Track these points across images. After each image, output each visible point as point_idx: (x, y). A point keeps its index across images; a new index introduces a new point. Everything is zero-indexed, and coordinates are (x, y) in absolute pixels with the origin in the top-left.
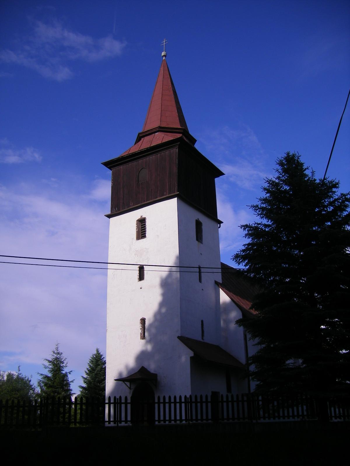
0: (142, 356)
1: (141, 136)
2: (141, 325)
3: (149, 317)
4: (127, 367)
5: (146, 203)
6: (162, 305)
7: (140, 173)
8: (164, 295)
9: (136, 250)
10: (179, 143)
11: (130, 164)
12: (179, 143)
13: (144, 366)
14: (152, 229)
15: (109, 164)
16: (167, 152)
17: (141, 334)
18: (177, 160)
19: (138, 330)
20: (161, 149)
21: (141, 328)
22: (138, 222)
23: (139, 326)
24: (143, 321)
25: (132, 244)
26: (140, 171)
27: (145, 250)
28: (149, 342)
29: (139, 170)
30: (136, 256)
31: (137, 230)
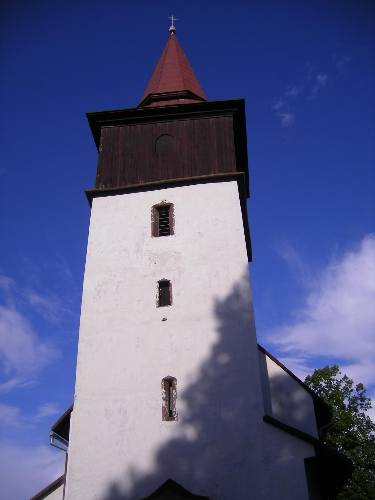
0: (169, 453)
1: (152, 98)
2: (165, 391)
3: (185, 373)
4: (132, 472)
5: (171, 180)
6: (217, 349)
7: (164, 136)
8: (222, 330)
9: (151, 253)
10: (237, 109)
11: (139, 126)
12: (237, 109)
13: (174, 479)
14: (188, 223)
15: (97, 121)
16: (212, 120)
17: (165, 409)
18: (232, 131)
19: (158, 400)
20: (204, 112)
21: (164, 396)
22: (155, 209)
23: (159, 393)
24: (169, 383)
25: (143, 242)
26: (159, 137)
27: (174, 254)
28: (187, 421)
29: (158, 136)
30: (153, 262)
31: (153, 221)
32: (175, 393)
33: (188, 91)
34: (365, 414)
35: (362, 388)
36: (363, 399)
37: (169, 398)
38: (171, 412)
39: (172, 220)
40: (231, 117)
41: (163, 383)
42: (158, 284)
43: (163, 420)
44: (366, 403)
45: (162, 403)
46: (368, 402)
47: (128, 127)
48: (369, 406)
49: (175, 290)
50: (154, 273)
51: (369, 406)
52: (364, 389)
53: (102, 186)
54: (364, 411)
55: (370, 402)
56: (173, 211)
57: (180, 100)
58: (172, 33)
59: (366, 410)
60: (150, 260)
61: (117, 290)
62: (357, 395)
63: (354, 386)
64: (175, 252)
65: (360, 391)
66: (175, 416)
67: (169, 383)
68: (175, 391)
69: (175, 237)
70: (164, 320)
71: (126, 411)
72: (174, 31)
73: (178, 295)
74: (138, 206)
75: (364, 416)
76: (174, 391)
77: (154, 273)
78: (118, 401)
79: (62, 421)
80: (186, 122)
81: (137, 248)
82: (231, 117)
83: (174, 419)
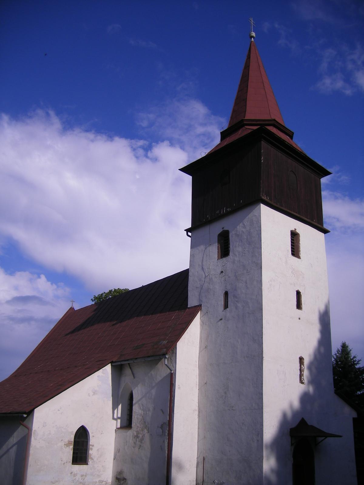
24: (301, 359)
66: (304, 382)
68: (304, 366)
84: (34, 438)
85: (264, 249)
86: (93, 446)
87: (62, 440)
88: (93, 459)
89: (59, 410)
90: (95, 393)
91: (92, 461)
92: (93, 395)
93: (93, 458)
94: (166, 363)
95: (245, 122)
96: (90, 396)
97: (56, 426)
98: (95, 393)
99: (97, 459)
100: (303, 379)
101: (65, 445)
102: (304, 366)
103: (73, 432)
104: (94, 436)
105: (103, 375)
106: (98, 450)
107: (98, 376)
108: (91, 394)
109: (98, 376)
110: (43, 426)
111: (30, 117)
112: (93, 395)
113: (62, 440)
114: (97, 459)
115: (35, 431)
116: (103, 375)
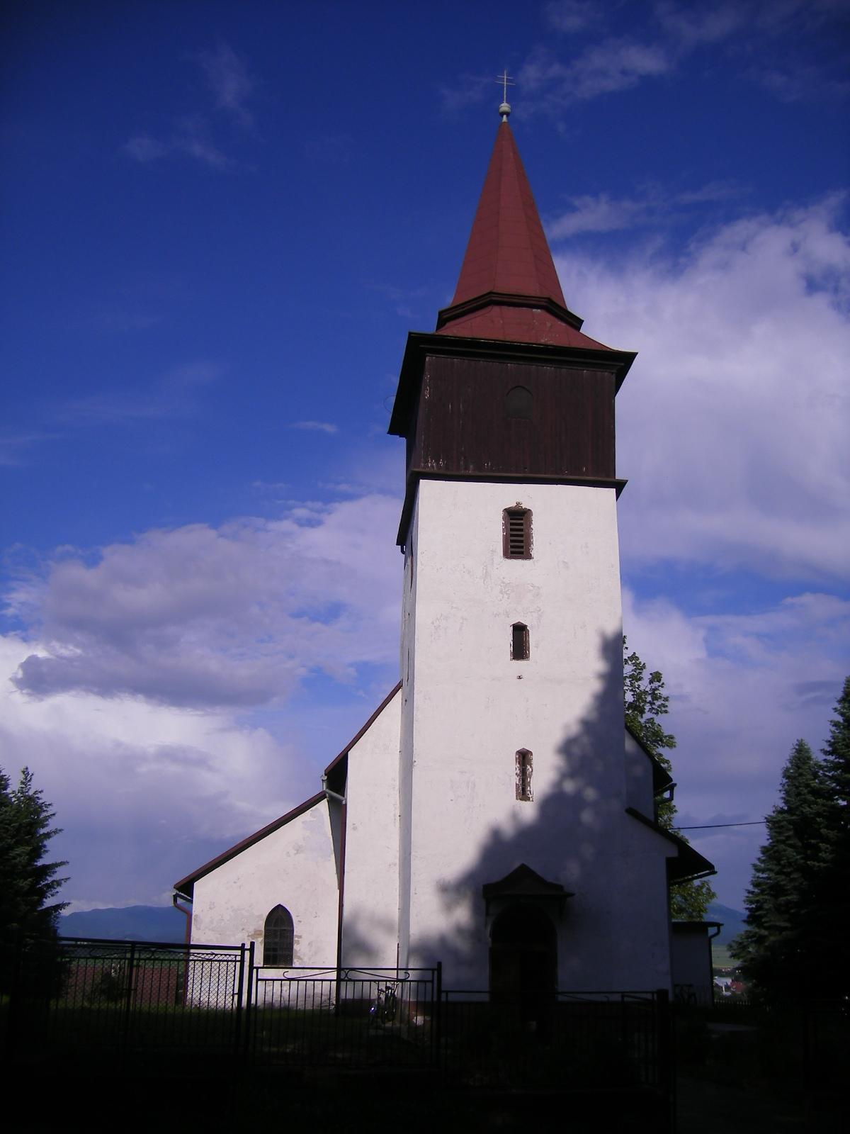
11: (482, 363)
22: (506, 514)
23: (513, 767)
24: (524, 758)
25: (493, 563)
30: (506, 596)
32: (530, 770)
33: (549, 299)
34: (655, 721)
35: (659, 681)
36: (655, 697)
37: (524, 776)
38: (524, 790)
39: (529, 536)
40: (612, 373)
41: (517, 756)
42: (512, 627)
43: (517, 799)
44: (660, 703)
45: (515, 780)
46: (663, 702)
47: (466, 361)
48: (663, 709)
49: (533, 639)
50: (507, 612)
51: (663, 709)
52: (661, 682)
53: (432, 461)
54: (654, 716)
55: (667, 703)
56: (530, 522)
57: (534, 310)
58: (505, 116)
59: (657, 713)
60: (501, 592)
61: (460, 629)
62: (648, 689)
63: (646, 675)
64: (533, 586)
65: (656, 684)
66: (530, 796)
67: (524, 758)
68: (531, 767)
69: (534, 563)
70: (520, 678)
71: (475, 786)
72: (507, 114)
73: (537, 647)
74: (485, 502)
75: (653, 724)
76: (529, 767)
77: (507, 612)
78: (465, 772)
79: (337, 761)
80: (548, 369)
81: (485, 571)
82: (612, 373)
83: (529, 799)
84: (197, 927)
85: (422, 565)
86: (300, 937)
87: (243, 929)
88: (301, 959)
89: (235, 882)
90: (298, 850)
91: (300, 961)
92: (295, 854)
93: (302, 957)
94: (784, 838)
95: (445, 317)
96: (289, 856)
97: (232, 907)
98: (298, 850)
99: (310, 959)
100: (529, 792)
101: (248, 936)
102: (531, 767)
103: (262, 915)
104: (300, 922)
105: (312, 819)
106: (310, 944)
107: (303, 822)
108: (293, 852)
109: (303, 822)
110: (210, 908)
111: (779, 222)
112: (295, 854)
113: (243, 929)
114: (310, 959)
115: (196, 916)
116: (312, 819)
